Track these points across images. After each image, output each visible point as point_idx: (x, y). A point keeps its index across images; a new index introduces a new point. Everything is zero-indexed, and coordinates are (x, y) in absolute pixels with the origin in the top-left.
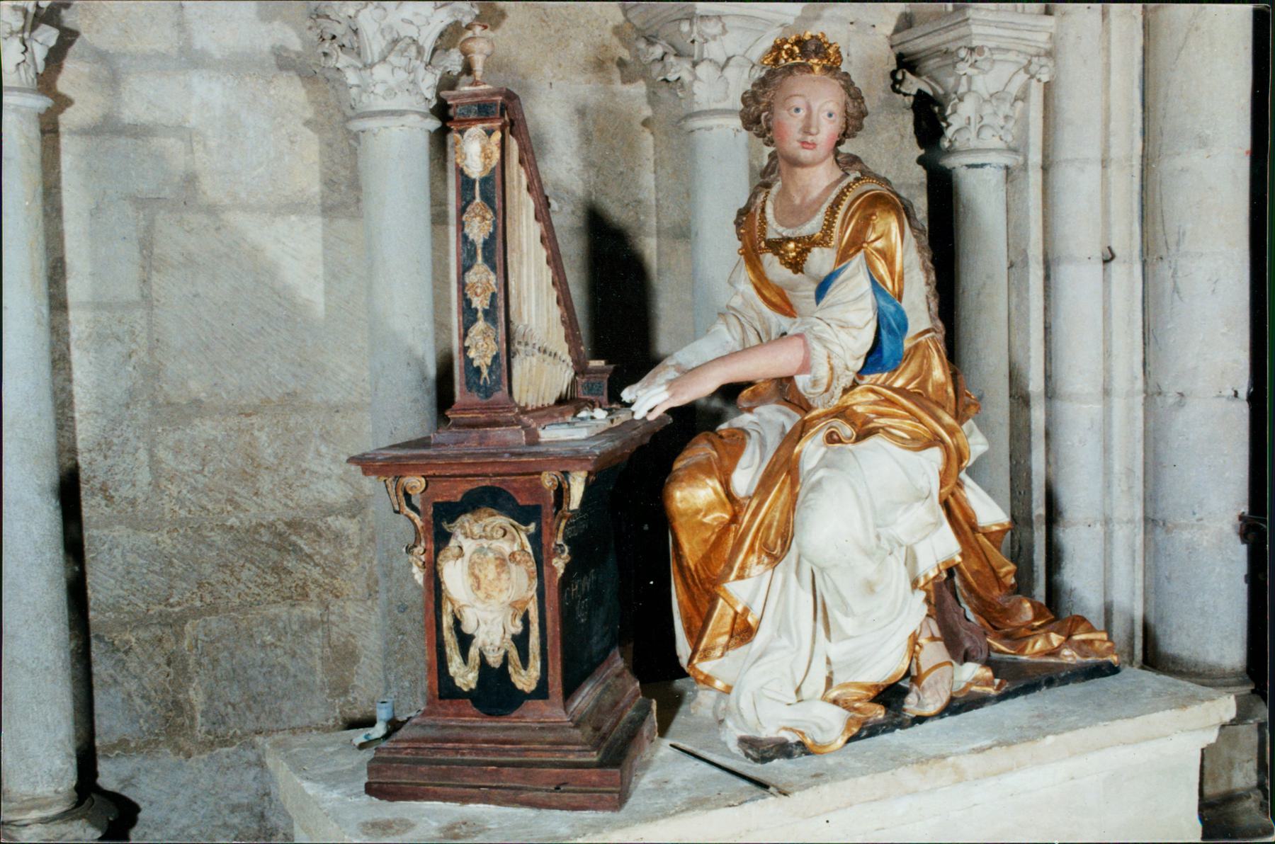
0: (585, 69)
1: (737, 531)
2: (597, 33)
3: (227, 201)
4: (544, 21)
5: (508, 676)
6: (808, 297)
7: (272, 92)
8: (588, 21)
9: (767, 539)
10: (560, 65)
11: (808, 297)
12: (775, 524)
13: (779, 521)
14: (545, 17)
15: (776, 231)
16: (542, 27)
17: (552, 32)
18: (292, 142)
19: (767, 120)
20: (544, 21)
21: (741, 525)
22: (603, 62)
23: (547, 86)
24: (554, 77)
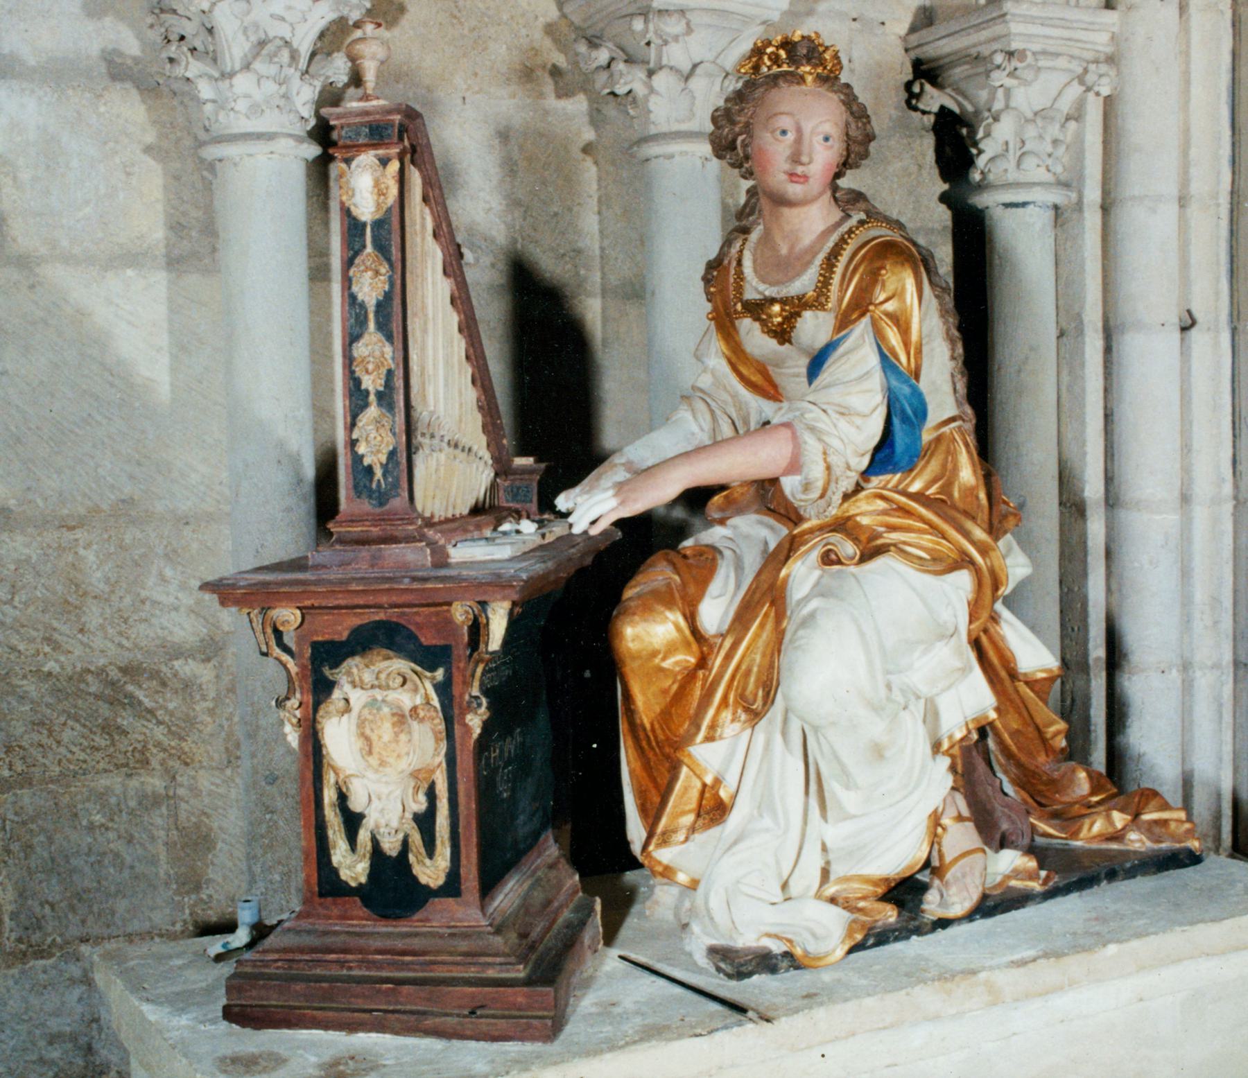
0: (508, 79)
1: (705, 679)
2: (524, 32)
3: (43, 251)
4: (455, 17)
5: (408, 867)
6: (797, 375)
7: (102, 109)
8: (512, 17)
9: (744, 689)
10: (476, 74)
11: (797, 375)
12: (755, 669)
13: (759, 666)
14: (458, 15)
15: (756, 289)
16: (453, 25)
17: (466, 32)
18: (128, 174)
19: (745, 146)
20: (455, 17)
21: (710, 671)
22: (532, 70)
23: (460, 101)
24: (468, 89)
